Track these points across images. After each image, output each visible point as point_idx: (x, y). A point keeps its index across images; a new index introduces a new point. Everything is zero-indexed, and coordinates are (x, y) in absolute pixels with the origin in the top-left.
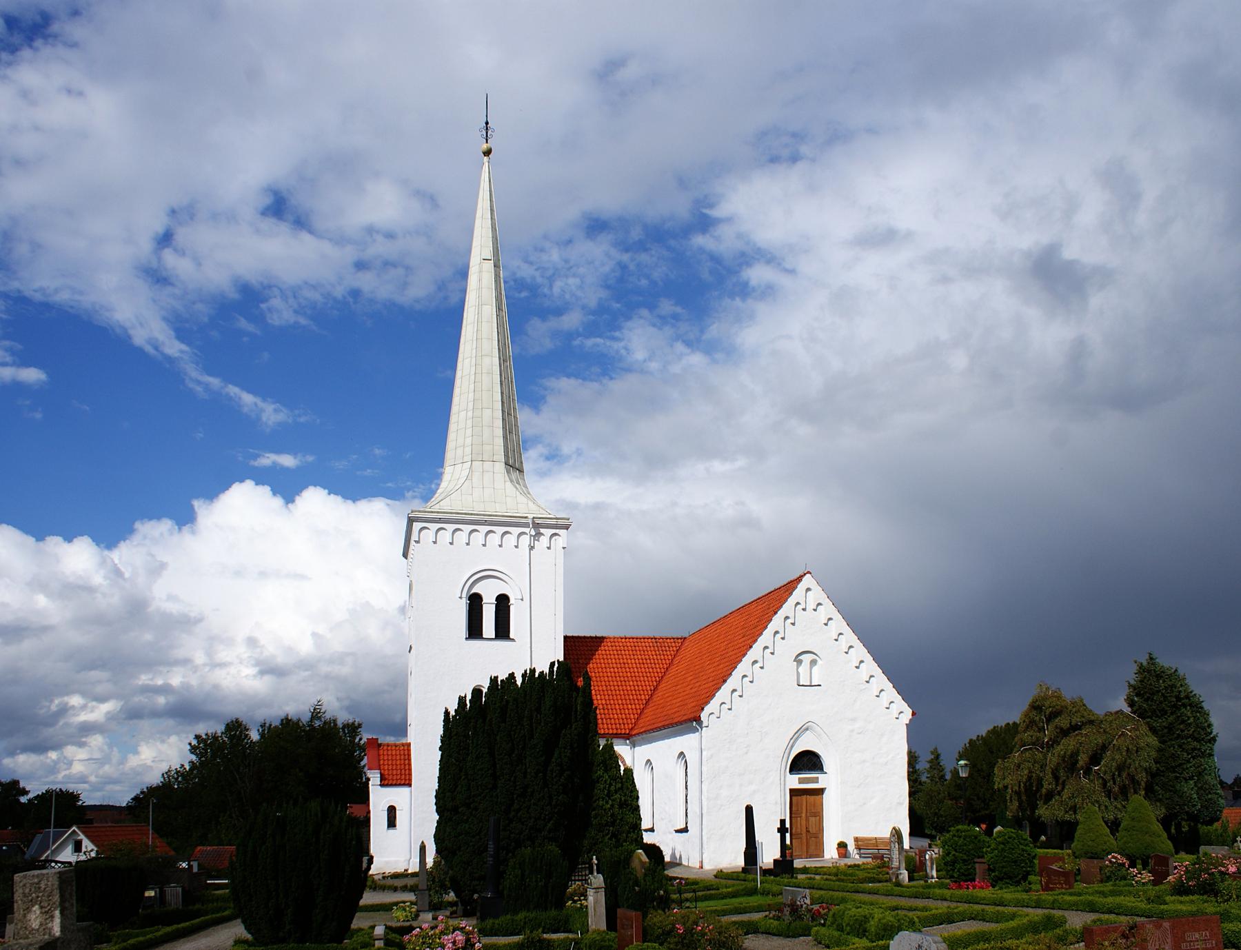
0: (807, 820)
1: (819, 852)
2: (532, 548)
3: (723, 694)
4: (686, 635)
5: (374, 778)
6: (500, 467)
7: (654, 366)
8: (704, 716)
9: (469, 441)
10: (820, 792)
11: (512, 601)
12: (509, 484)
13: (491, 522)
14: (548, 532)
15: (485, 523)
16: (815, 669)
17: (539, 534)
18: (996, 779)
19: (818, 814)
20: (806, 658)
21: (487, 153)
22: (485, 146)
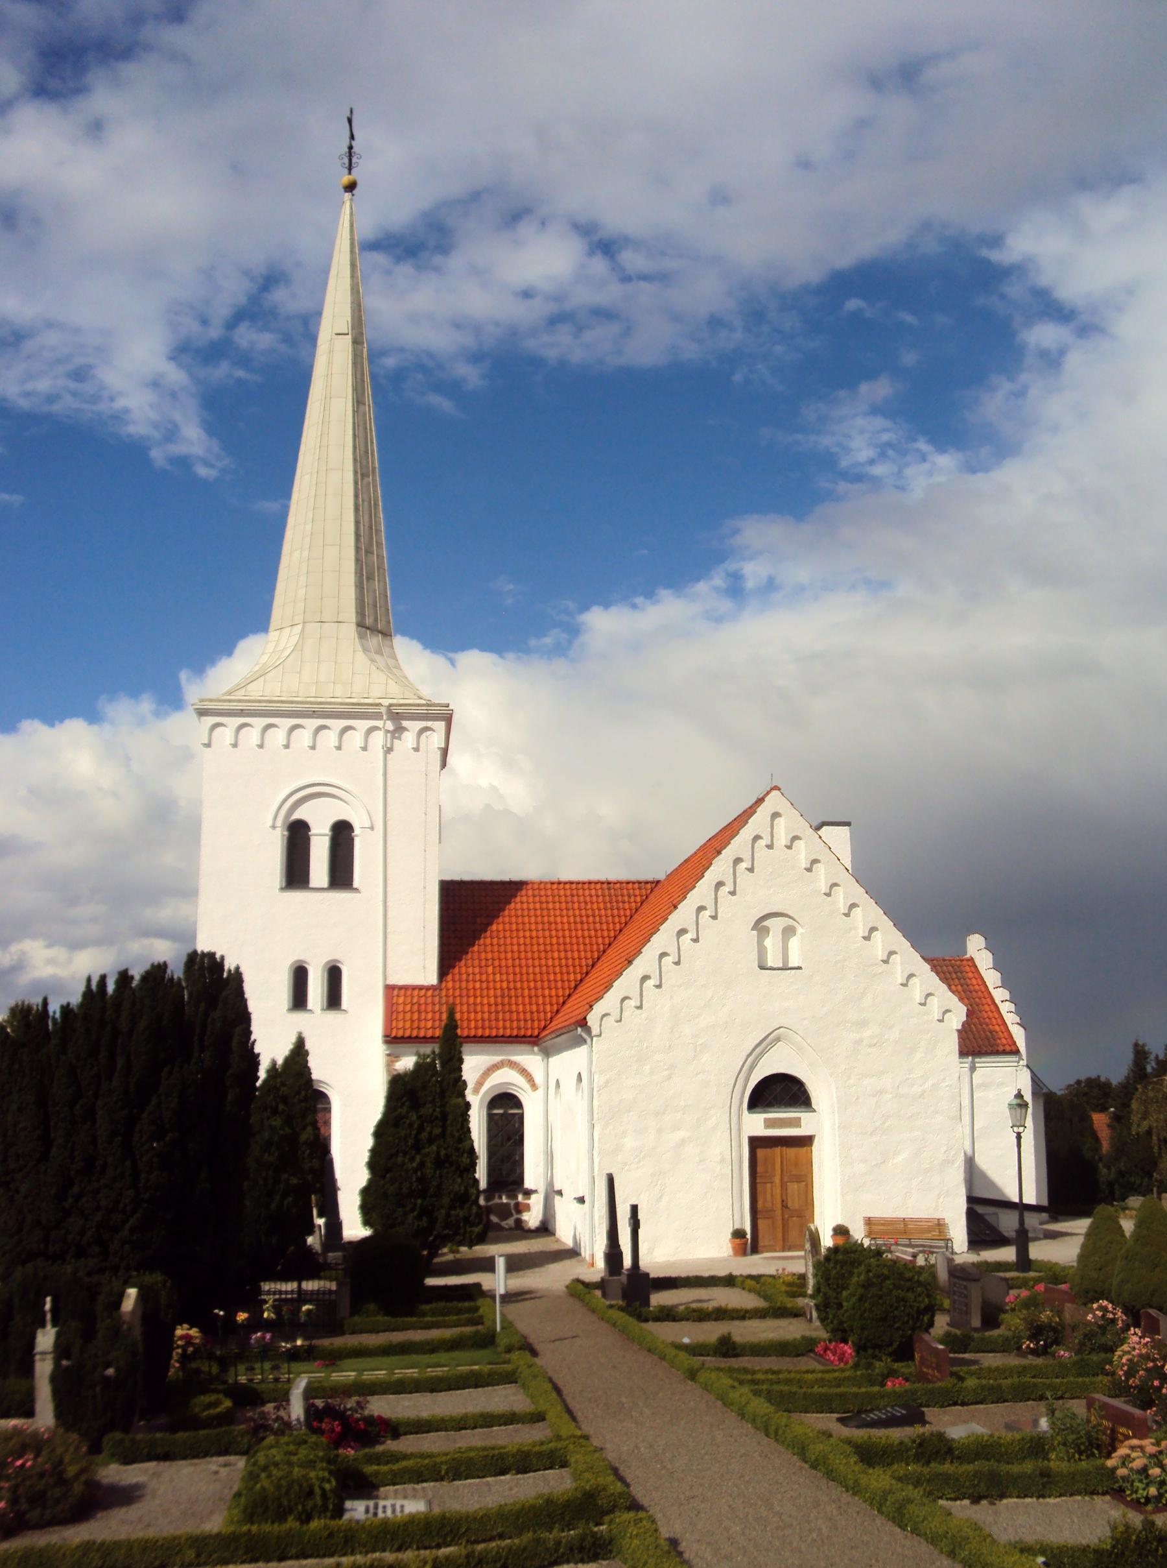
0: (783, 1186)
2: (389, 750)
4: (661, 876)
7: (878, 470)
8: (593, 1019)
9: (302, 592)
10: (806, 1141)
11: (357, 831)
12: (360, 656)
14: (414, 726)
15: (314, 714)
16: (794, 943)
17: (399, 730)
18: (1135, 1118)
19: (804, 1178)
22: (346, 179)
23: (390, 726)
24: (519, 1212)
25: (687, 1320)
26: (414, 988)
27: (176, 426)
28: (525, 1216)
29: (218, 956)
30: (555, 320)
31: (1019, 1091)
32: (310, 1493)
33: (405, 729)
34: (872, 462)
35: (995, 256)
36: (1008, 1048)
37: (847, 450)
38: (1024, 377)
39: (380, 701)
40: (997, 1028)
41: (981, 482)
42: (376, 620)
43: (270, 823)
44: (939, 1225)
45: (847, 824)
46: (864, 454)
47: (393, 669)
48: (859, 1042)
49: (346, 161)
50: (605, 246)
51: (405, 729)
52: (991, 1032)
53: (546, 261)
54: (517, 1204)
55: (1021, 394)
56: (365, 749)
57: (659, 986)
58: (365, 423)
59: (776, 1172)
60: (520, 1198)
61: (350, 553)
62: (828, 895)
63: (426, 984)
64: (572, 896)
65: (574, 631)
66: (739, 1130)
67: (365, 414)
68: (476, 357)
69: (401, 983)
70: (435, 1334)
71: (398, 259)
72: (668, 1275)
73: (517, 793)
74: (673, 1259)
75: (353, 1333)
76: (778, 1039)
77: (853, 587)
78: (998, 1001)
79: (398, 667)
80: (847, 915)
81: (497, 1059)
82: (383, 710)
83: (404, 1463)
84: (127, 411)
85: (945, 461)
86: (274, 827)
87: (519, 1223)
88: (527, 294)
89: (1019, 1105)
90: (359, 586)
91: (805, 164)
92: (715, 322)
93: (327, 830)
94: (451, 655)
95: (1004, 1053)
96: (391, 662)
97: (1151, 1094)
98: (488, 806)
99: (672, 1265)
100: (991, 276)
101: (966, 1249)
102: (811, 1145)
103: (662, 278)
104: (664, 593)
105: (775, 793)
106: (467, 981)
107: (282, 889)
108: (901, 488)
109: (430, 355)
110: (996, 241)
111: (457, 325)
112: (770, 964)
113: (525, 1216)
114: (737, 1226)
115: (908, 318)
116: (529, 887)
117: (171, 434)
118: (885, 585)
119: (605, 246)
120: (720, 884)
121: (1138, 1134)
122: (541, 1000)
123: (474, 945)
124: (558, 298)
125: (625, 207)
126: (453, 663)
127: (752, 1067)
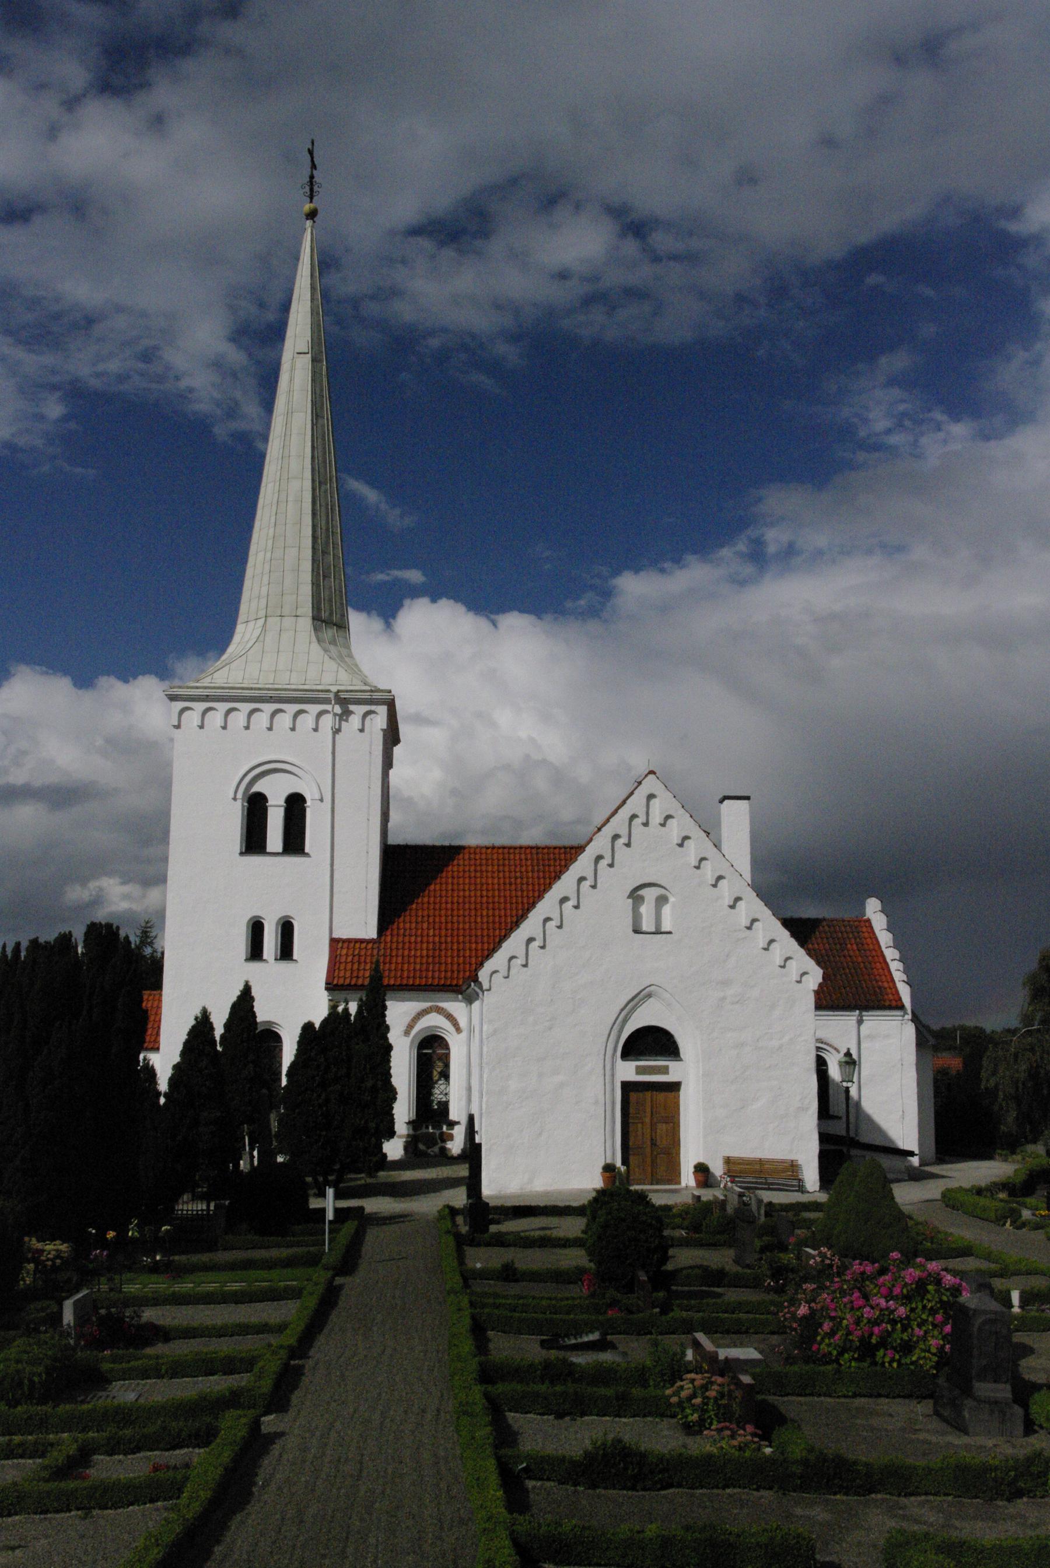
0: (653, 1126)
1: (674, 1175)
2: (337, 731)
6: (306, 623)
7: (895, 439)
8: (483, 975)
10: (674, 1087)
12: (315, 646)
13: (279, 698)
14: (359, 710)
16: (666, 910)
17: (346, 714)
18: (984, 1074)
19: (672, 1120)
21: (312, 215)
22: (307, 207)
23: (338, 709)
24: (444, 1141)
25: (515, 1246)
27: (237, 404)
28: (449, 1145)
29: (114, 927)
30: (589, 301)
31: (849, 1050)
32: (20, 1384)
33: (352, 712)
34: (888, 432)
35: (1013, 227)
36: (894, 1003)
37: (866, 421)
38: (1039, 346)
39: (328, 688)
40: (886, 985)
41: (995, 449)
42: (331, 614)
43: (232, 795)
44: (792, 1166)
45: (748, 798)
46: (881, 424)
47: (346, 658)
48: (724, 998)
49: (307, 189)
50: (635, 227)
51: (352, 712)
52: (880, 988)
53: (579, 244)
54: (442, 1134)
55: (1036, 362)
56: (316, 730)
57: (543, 947)
58: (324, 436)
59: (647, 1115)
60: (445, 1128)
61: (308, 553)
62: (698, 867)
63: (367, 938)
64: (504, 859)
65: (607, 594)
66: (613, 1075)
67: (323, 426)
68: (515, 337)
69: (345, 937)
70: (275, 1253)
71: (442, 244)
72: (528, 1204)
73: (554, 744)
74: (549, 1189)
75: (225, 1249)
76: (649, 996)
77: (870, 552)
78: (888, 960)
79: (350, 656)
80: (715, 886)
81: (428, 1004)
82: (332, 696)
84: (191, 390)
85: (959, 429)
86: (235, 799)
87: (444, 1151)
88: (563, 275)
89: (847, 1063)
90: (315, 584)
91: (829, 142)
92: (740, 299)
93: (282, 802)
94: (493, 617)
95: (890, 1008)
96: (344, 651)
97: (1000, 1053)
98: (528, 756)
99: (547, 1194)
100: (1010, 247)
101: (818, 1189)
102: (679, 1090)
103: (690, 258)
104: (690, 558)
105: (651, 776)
106: (404, 936)
107: (241, 854)
108: (918, 457)
109: (473, 336)
110: (1015, 212)
111: (498, 307)
112: (663, 930)
113: (449, 1145)
114: (609, 1161)
115: (929, 292)
116: (466, 851)
117: (232, 412)
118: (900, 549)
119: (635, 227)
120: (599, 858)
121: (987, 1089)
122: (468, 953)
123: (412, 903)
124: (595, 278)
125: (655, 188)
126: (494, 624)
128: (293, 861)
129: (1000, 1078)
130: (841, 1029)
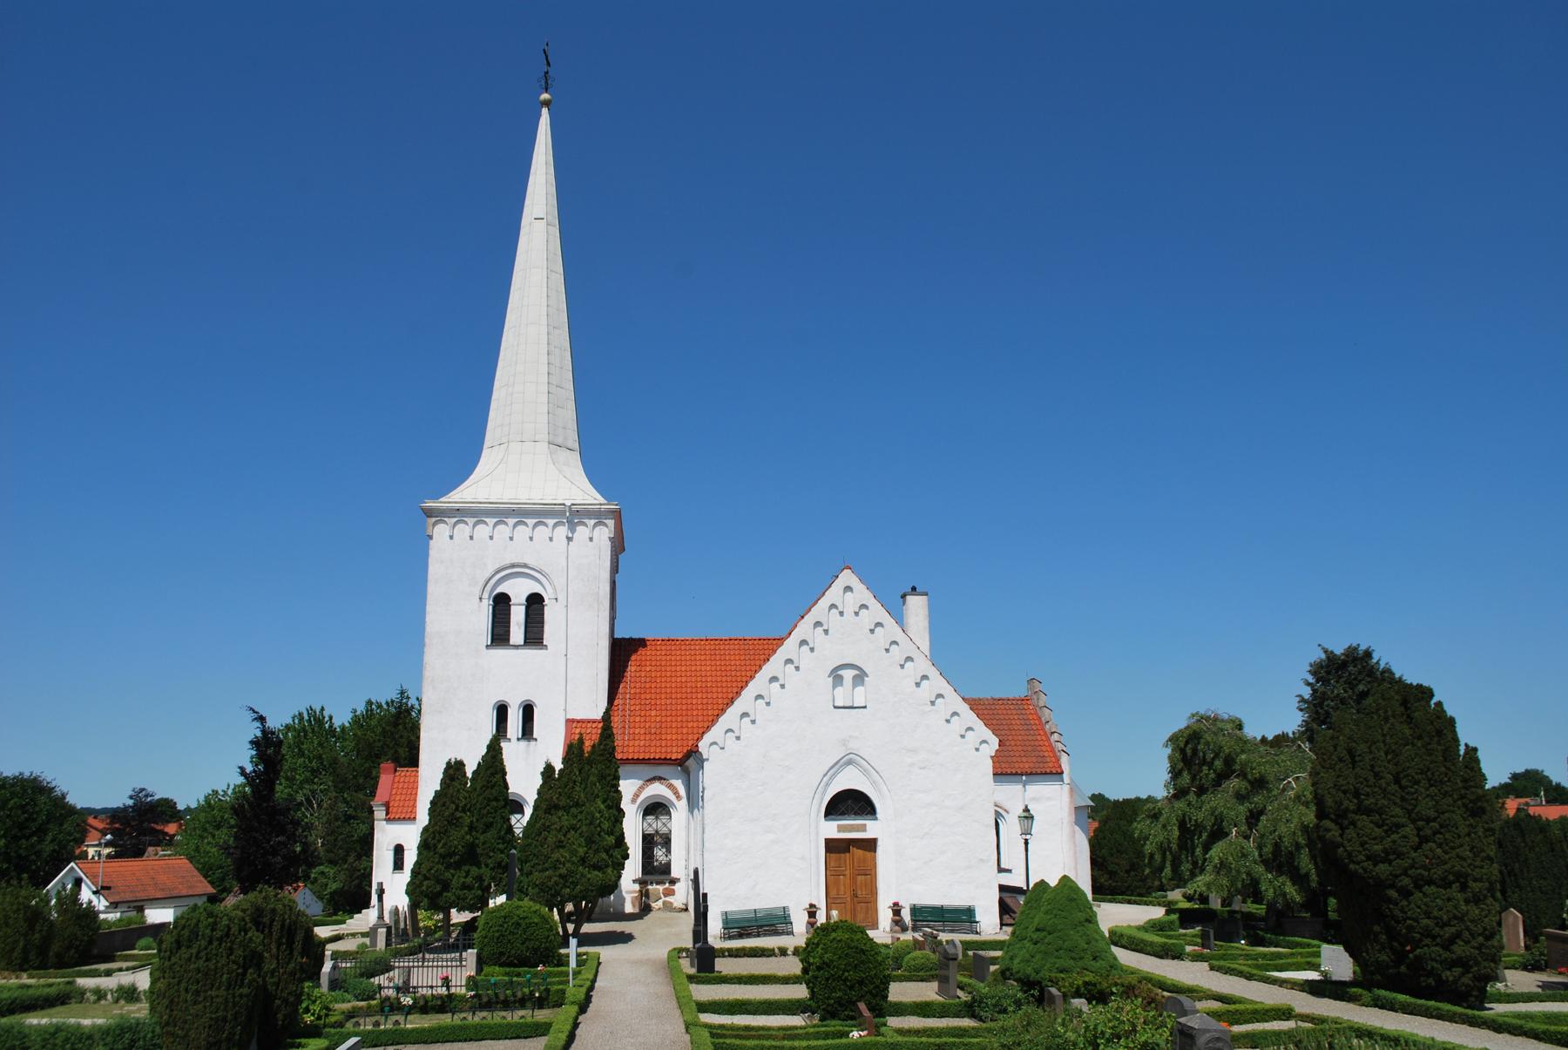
3: (730, 717)
5: (379, 813)
8: (703, 746)
10: (870, 845)
19: (869, 872)
20: (848, 675)
26: (589, 721)
48: (912, 765)
83: (1237, 1006)
93: (523, 600)
127: (827, 785)
128: (532, 653)
129: (1154, 836)
130: (1014, 796)
